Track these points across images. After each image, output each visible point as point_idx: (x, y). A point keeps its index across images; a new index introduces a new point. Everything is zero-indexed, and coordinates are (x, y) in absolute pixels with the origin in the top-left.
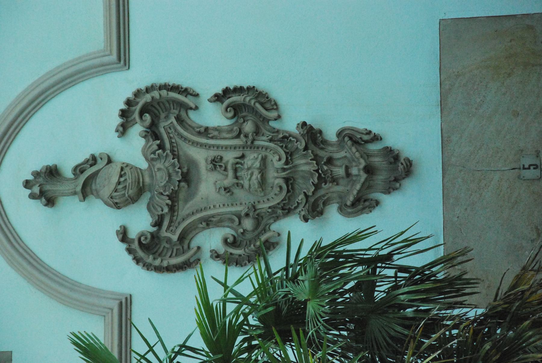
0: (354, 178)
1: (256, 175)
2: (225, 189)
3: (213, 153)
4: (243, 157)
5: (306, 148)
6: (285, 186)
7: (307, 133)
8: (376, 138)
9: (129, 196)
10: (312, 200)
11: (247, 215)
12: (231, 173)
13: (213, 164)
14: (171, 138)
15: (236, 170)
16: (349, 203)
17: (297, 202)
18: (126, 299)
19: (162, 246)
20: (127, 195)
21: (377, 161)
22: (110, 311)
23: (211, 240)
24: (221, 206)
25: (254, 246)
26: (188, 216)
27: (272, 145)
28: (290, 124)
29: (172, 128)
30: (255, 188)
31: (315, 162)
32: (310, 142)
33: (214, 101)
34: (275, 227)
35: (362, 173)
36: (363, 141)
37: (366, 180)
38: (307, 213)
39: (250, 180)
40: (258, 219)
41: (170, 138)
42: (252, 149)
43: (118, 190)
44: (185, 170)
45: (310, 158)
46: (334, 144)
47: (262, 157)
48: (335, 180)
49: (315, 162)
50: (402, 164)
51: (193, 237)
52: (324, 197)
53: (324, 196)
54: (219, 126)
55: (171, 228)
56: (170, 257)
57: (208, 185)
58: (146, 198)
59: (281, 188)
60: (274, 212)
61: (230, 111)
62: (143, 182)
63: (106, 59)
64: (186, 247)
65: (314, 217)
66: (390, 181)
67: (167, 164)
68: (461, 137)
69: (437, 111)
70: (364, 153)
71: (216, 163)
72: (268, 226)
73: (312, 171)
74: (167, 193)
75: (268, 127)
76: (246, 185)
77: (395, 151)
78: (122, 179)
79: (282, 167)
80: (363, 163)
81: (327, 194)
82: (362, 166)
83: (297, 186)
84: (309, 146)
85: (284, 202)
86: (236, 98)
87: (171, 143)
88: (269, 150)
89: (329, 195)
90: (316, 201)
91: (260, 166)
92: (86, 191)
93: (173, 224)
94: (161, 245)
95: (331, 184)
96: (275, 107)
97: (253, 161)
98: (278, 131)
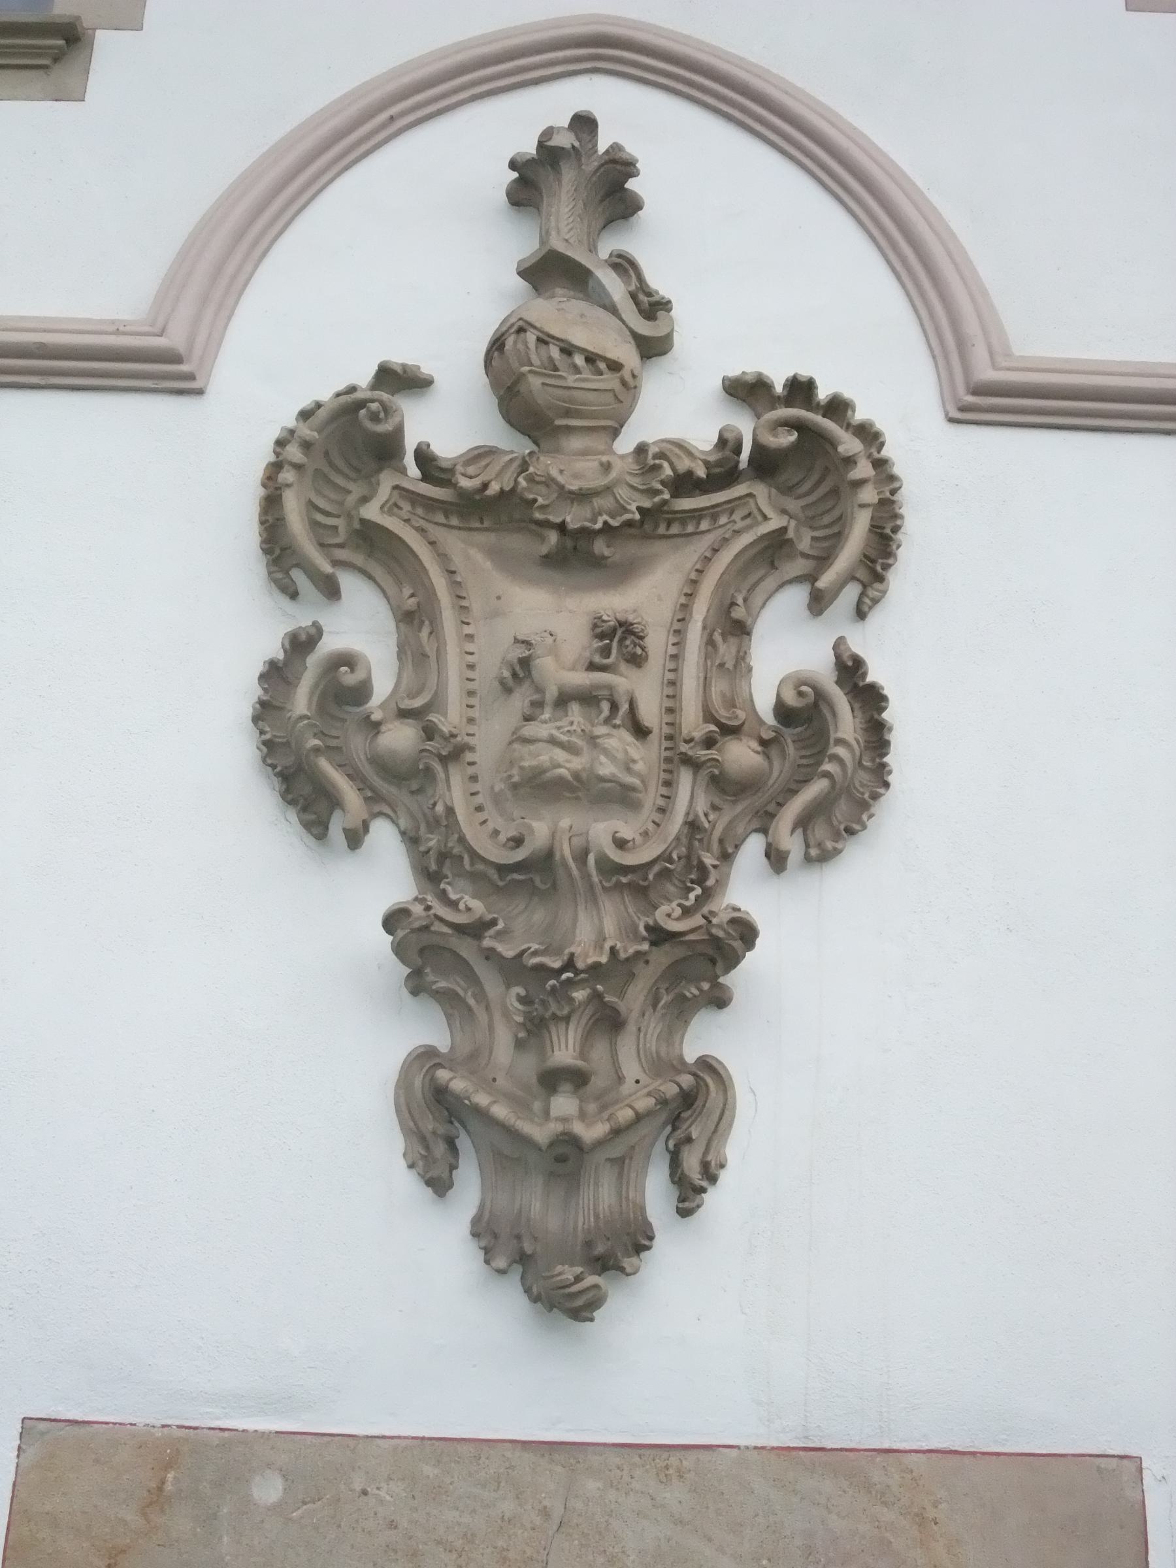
0: (537, 1106)
1: (567, 764)
2: (525, 663)
3: (657, 642)
4: (640, 731)
5: (659, 936)
6: (520, 855)
7: (715, 941)
8: (688, 1196)
10: (466, 948)
11: (430, 732)
12: (581, 679)
13: (614, 630)
14: (714, 518)
15: (588, 698)
16: (443, 1075)
18: (191, 377)
19: (351, 486)
20: (526, 369)
21: (600, 1195)
22: (156, 330)
23: (361, 625)
24: (470, 658)
25: (317, 750)
26: (443, 558)
28: (747, 889)
29: (748, 521)
30: (522, 759)
31: (604, 959)
32: (679, 952)
33: (838, 657)
34: (384, 837)
35: (555, 1127)
36: (678, 1147)
37: (526, 1141)
38: (417, 925)
39: (553, 741)
41: (713, 512)
42: (664, 766)
43: (543, 348)
44: (600, 547)
45: (619, 945)
47: (633, 789)
48: (535, 1030)
50: (578, 1279)
52: (474, 996)
53: (481, 995)
54: (750, 670)
55: (406, 506)
56: (312, 506)
57: (553, 618)
58: (514, 444)
59: (518, 842)
60: (434, 824)
61: (801, 694)
62: (569, 429)
63: (979, 355)
64: (342, 554)
65: (399, 950)
66: (518, 1237)
67: (622, 493)
68: (680, 1522)
69: (783, 1433)
70: (633, 1148)
71: (619, 639)
72: (388, 810)
73: (572, 949)
74: (523, 482)
75: (740, 830)
76: (530, 730)
77: (634, 1260)
78: (579, 360)
80: (591, 1132)
81: (488, 1008)
82: (578, 1128)
84: (667, 947)
86: (847, 723)
87: (696, 515)
88: (657, 817)
91: (602, 779)
92: (548, 271)
93: (420, 511)
94: (355, 481)
96: (814, 852)
97: (620, 756)
98: (727, 857)
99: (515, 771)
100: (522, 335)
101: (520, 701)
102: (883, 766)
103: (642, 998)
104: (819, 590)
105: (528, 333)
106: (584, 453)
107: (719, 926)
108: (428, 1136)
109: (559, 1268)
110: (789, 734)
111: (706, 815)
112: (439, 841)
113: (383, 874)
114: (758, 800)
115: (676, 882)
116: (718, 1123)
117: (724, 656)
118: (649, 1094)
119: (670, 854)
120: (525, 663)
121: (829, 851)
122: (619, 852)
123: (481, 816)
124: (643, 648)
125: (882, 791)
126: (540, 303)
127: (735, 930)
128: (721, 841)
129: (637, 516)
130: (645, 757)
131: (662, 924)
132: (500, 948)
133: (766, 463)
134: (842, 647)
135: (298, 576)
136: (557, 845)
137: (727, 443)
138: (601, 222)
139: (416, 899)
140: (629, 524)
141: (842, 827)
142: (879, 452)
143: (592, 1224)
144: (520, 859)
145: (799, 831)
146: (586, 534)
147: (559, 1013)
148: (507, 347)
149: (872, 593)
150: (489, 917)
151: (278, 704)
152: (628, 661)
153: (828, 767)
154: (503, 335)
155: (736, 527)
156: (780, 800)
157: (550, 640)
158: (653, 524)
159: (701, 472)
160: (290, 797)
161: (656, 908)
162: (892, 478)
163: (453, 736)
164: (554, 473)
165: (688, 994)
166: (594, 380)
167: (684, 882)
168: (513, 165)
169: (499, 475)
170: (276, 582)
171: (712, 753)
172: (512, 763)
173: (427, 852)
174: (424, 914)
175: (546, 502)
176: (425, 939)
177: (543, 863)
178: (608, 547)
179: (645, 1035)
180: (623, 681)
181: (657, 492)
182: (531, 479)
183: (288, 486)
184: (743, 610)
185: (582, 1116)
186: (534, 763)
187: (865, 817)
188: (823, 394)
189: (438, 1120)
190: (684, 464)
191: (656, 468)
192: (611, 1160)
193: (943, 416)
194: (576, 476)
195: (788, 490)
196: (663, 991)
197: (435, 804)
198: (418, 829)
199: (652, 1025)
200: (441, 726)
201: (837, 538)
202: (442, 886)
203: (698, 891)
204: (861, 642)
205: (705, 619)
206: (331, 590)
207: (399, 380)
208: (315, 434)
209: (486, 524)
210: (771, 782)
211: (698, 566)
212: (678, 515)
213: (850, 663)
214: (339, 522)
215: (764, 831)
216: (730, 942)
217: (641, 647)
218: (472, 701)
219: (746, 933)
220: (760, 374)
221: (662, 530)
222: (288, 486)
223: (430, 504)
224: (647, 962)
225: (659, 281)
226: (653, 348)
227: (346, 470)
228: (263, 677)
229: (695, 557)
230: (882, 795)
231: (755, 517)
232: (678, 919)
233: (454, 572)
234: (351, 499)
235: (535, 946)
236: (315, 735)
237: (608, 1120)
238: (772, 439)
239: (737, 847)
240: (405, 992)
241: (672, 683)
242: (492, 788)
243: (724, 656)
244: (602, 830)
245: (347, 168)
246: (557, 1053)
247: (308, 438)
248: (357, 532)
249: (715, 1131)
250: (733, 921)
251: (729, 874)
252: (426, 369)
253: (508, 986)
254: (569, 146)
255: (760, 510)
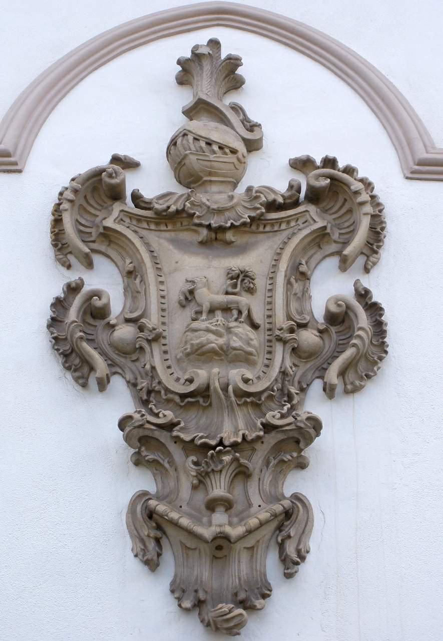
0: (205, 519)
2: (191, 292)
3: (261, 283)
5: (268, 428)
6: (192, 388)
8: (291, 565)
9: (186, 156)
10: (163, 436)
11: (141, 329)
12: (222, 298)
14: (288, 222)
15: (226, 309)
16: (153, 503)
17: (159, 412)
18: (16, 164)
19: (97, 213)
20: (188, 152)
21: (240, 568)
23: (105, 280)
25: (81, 338)
26: (147, 245)
27: (275, 372)
31: (239, 440)
32: (281, 436)
34: (118, 384)
36: (283, 541)
38: (137, 424)
39: (208, 330)
40: (133, 351)
43: (197, 143)
46: (276, 487)
47: (251, 354)
48: (201, 481)
49: (239, 440)
50: (230, 611)
51: (113, 260)
52: (169, 462)
53: (172, 462)
54: (310, 297)
55: (127, 220)
56: (77, 220)
57: (207, 271)
59: (191, 381)
61: (339, 306)
65: (127, 439)
66: (196, 591)
67: (240, 209)
70: (258, 541)
71: (241, 280)
72: (120, 371)
73: (222, 435)
75: (309, 375)
76: (195, 325)
79: (231, 381)
80: (235, 532)
82: (228, 529)
83: (194, 417)
84: (273, 434)
85: (163, 392)
86: (363, 319)
87: (279, 221)
89: (172, 472)
90: (161, 446)
91: (235, 349)
93: (134, 222)
94: (100, 211)
95: (194, 474)
98: (303, 390)
99: (188, 346)
100: (186, 137)
101: (189, 312)
102: (383, 343)
103: (260, 461)
104: (345, 256)
105: (189, 136)
106: (220, 192)
107: (301, 421)
108: (145, 539)
109: (220, 606)
110: (333, 329)
111: (291, 368)
112: (148, 384)
113: (120, 401)
114: (318, 362)
115: (276, 402)
116: (305, 528)
117: (296, 289)
118: (266, 512)
119: (273, 387)
120: (191, 292)
121: (357, 386)
122: (245, 385)
123: (170, 371)
124: (254, 284)
125: (384, 355)
126: (194, 122)
127: (310, 424)
128: (299, 382)
129: (249, 220)
130: (256, 339)
131: (270, 421)
132: (182, 436)
133: (314, 196)
134: (359, 284)
135: (72, 259)
136: (211, 382)
137: (294, 188)
138: (223, 90)
139: (136, 412)
140: (244, 224)
141: (363, 374)
142: (372, 192)
143: (238, 583)
144: (192, 389)
145: (341, 377)
146: (221, 229)
147: (215, 469)
148: (178, 143)
149: (372, 259)
150: (176, 420)
151: (59, 319)
152: (246, 291)
153: (354, 341)
154: (176, 136)
155: (299, 228)
156: (329, 361)
157: (205, 280)
158: (255, 224)
159: (281, 200)
160: (67, 365)
161: (265, 415)
162: (379, 204)
163: (154, 329)
164: (204, 200)
165: (285, 459)
166: (222, 157)
167: (280, 402)
168: (179, 62)
169: (175, 203)
170: (59, 260)
171: (294, 336)
172: (186, 342)
173: (141, 389)
174: (140, 418)
175: (201, 215)
176: (141, 432)
177: (204, 392)
178: (234, 236)
179: (263, 481)
180: (244, 300)
181: (258, 209)
182: (192, 203)
183: (66, 210)
184: (306, 267)
185: (230, 524)
186: (198, 341)
187: (375, 369)
188: (341, 164)
189: (152, 531)
190: (271, 197)
191: (257, 197)
192: (248, 548)
193: (403, 176)
194: (216, 203)
195: (325, 211)
196: (272, 458)
197: (145, 365)
198: (136, 379)
199: (266, 477)
200: (147, 325)
201: (353, 232)
202: (150, 406)
203: (289, 406)
204: (367, 282)
205: (286, 271)
206: (89, 265)
207: (124, 163)
208: (80, 185)
209: (170, 227)
210: (326, 350)
211: (281, 246)
212: (269, 222)
213: (363, 292)
214: (93, 231)
215: (321, 377)
216: (308, 430)
217: (252, 283)
218: (164, 314)
219: (316, 425)
220: (308, 156)
221: (261, 229)
222: (66, 210)
223: (139, 219)
224: (262, 442)
225: (254, 116)
226: (253, 146)
227: (96, 206)
228: (53, 305)
229: (279, 242)
230: (385, 357)
231: (310, 222)
232: (278, 419)
233: (153, 252)
234: (98, 220)
235: (201, 434)
236: (81, 331)
237: (245, 525)
238: (317, 183)
239: (308, 385)
240: (131, 464)
241: (270, 303)
242: (176, 357)
243: (296, 289)
244: (235, 375)
245: (96, 69)
246: (215, 490)
247: (76, 187)
248: (101, 234)
249: (303, 532)
250: (309, 419)
251: (304, 399)
252: (137, 158)
253: (187, 457)
254: (207, 53)
255: (312, 218)
